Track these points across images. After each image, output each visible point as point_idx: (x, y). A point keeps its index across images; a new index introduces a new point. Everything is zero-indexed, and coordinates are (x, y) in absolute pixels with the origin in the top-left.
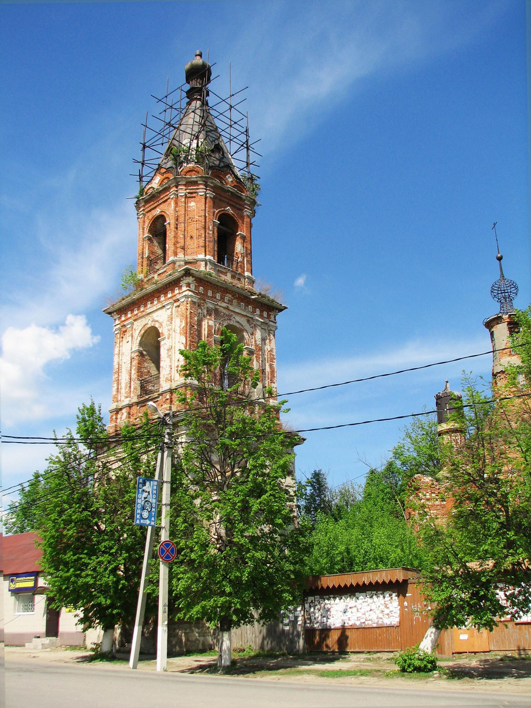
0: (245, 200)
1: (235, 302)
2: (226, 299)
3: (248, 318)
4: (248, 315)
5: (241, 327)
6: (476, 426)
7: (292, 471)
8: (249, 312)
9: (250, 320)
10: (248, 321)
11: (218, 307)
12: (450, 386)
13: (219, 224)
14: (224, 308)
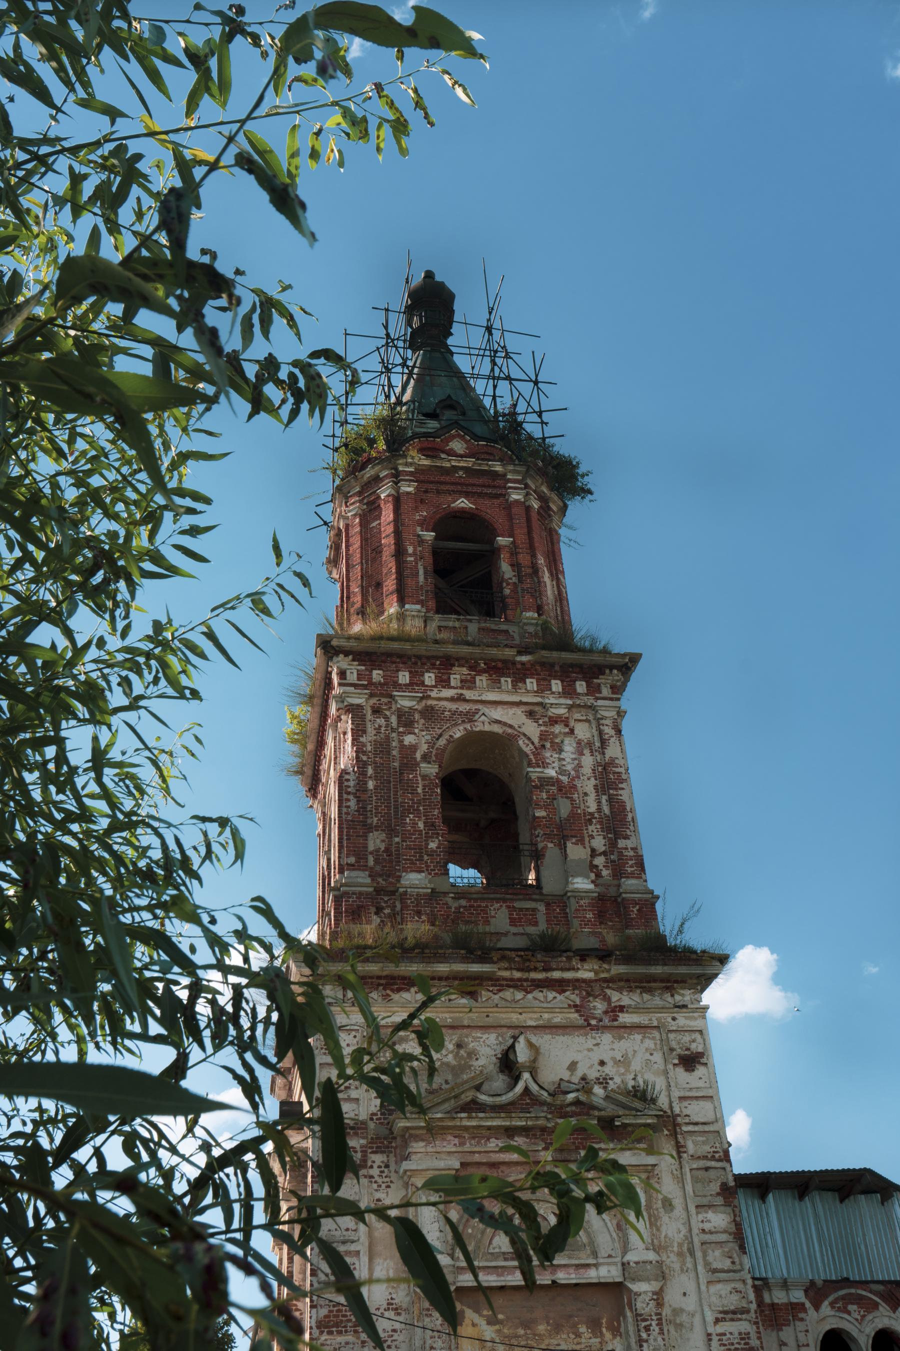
0: (505, 475)
1: (482, 680)
2: (455, 680)
3: (528, 708)
4: (525, 700)
5: (510, 731)
6: (599, 716)
7: (701, 1055)
8: (528, 692)
9: (537, 708)
10: (531, 714)
11: (430, 702)
12: (316, 828)
13: (436, 538)
14: (452, 699)
